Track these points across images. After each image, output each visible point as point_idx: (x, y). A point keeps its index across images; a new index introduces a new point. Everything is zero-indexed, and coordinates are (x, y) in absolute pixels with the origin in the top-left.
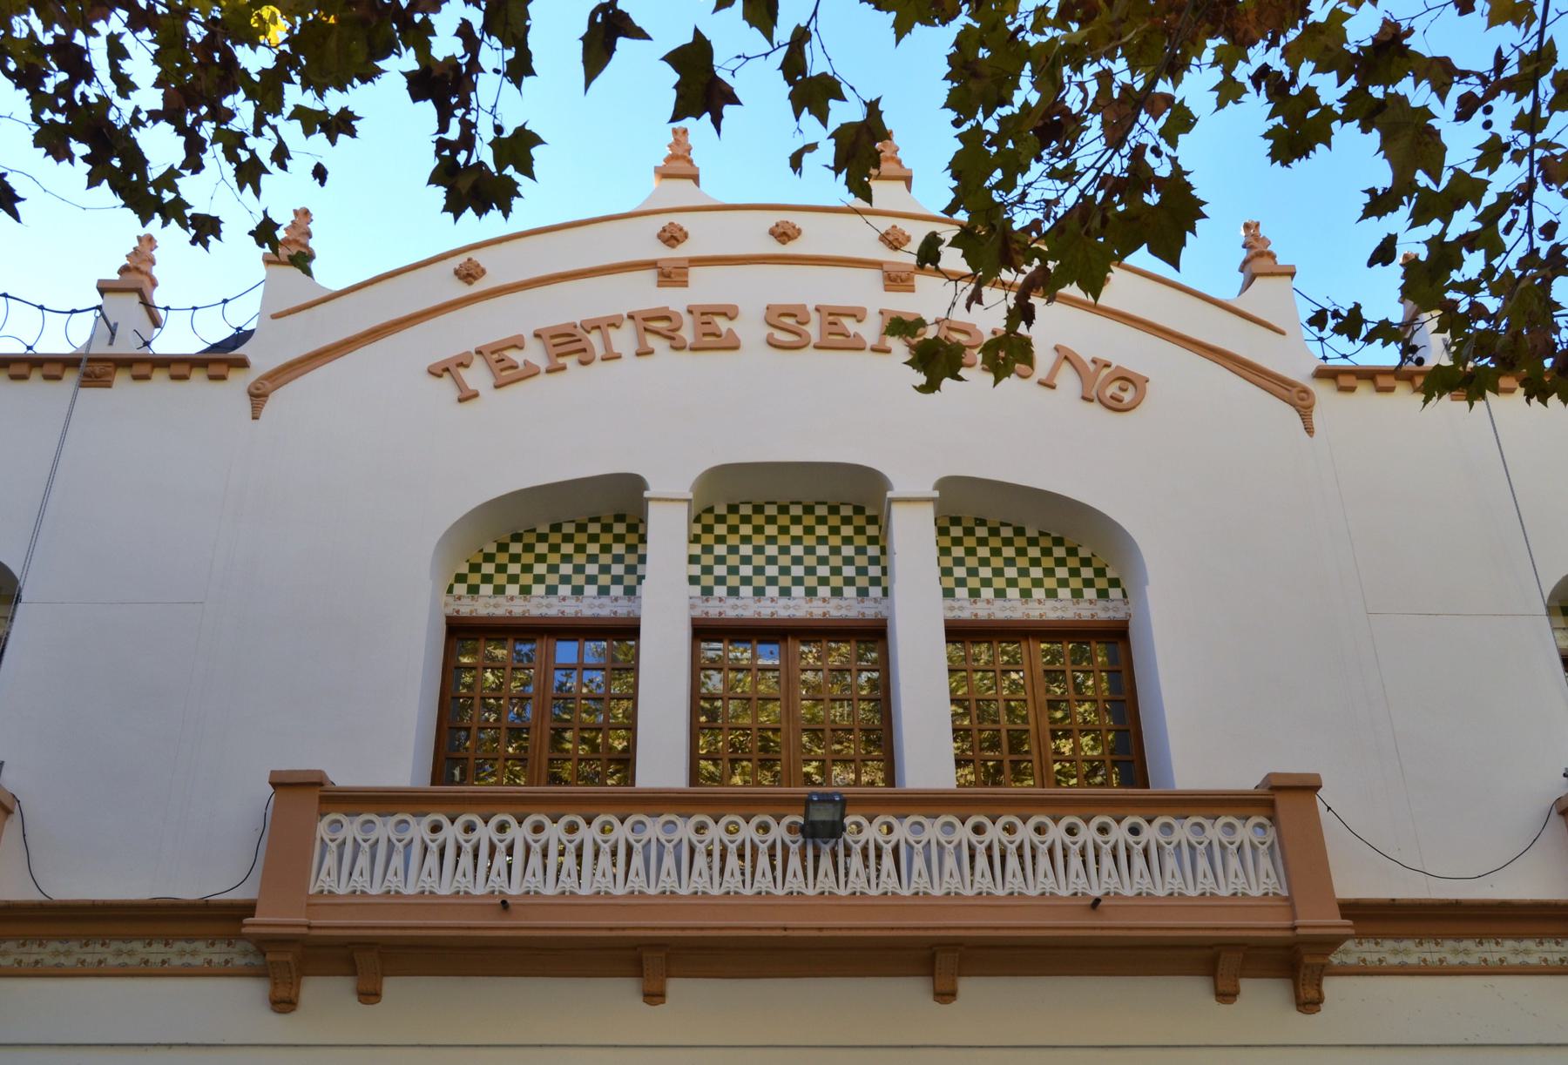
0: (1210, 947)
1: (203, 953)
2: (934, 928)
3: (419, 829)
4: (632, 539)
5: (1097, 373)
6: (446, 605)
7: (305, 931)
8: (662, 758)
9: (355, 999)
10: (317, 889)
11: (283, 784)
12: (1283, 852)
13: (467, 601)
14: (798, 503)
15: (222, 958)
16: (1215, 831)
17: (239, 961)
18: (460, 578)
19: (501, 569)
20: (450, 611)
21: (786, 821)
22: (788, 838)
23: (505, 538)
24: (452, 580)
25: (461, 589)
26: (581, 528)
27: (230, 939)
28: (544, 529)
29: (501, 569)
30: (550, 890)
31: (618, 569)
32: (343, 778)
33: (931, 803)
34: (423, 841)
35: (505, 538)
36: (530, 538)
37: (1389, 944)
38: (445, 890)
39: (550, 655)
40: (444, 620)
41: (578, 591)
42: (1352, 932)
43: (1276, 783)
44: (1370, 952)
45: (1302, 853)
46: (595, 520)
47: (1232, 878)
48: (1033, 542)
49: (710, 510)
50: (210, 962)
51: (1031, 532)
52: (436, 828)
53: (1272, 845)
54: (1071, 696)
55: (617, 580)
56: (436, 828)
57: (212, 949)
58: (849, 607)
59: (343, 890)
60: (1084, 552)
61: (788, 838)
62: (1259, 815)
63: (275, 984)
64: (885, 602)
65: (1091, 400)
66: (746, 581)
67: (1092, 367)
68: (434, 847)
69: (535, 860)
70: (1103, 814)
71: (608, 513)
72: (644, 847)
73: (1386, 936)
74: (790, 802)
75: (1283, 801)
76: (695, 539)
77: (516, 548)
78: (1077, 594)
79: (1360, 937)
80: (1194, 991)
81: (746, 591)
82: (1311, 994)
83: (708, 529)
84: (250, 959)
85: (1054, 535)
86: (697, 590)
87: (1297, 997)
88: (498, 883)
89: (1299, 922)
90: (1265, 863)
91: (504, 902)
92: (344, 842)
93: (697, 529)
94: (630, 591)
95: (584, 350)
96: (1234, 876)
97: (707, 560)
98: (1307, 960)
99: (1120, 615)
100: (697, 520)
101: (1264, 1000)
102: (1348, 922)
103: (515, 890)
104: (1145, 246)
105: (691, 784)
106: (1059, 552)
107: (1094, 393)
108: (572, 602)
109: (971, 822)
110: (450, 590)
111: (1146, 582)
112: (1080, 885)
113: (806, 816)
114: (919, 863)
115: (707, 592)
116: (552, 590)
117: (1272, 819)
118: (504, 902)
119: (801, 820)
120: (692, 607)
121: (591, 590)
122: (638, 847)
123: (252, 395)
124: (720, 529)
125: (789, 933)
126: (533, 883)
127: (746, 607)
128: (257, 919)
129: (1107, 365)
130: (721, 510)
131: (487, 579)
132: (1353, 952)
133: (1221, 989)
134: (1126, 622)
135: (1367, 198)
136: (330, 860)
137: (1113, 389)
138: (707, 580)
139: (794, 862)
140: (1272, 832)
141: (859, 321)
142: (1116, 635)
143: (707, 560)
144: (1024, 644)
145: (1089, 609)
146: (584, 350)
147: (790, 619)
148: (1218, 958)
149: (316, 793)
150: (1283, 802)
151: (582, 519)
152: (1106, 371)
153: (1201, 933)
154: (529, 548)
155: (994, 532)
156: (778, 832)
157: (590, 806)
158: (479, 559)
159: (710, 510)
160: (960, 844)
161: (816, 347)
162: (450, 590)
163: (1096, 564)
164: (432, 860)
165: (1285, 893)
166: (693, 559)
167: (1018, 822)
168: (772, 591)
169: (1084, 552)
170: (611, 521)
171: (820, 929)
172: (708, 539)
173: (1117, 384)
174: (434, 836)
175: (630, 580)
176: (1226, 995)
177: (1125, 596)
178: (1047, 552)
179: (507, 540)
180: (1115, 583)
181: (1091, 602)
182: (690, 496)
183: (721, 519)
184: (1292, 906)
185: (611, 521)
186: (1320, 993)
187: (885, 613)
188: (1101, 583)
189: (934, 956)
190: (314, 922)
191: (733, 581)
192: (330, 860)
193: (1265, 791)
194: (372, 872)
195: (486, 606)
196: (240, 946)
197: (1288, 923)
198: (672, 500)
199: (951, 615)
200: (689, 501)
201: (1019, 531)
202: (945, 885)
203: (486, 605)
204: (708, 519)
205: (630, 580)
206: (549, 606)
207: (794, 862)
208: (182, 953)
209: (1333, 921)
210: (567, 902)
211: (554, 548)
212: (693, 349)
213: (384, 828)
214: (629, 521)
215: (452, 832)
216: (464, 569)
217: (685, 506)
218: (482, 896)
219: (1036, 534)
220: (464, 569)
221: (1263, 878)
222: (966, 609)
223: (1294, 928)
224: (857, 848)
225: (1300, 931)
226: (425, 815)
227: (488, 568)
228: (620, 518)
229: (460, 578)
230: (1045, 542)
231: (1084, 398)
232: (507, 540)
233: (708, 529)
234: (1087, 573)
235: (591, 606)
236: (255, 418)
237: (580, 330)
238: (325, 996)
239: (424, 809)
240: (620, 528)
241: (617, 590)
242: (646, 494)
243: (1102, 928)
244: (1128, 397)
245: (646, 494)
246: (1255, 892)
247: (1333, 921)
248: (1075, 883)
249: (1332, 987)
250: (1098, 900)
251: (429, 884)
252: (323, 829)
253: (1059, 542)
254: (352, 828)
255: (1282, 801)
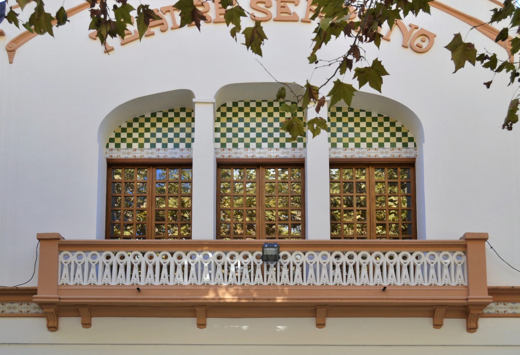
0: (432, 306)
1: (18, 308)
2: (316, 299)
3: (101, 258)
4: (188, 120)
5: (411, 32)
6: (106, 153)
7: (58, 300)
8: (203, 224)
9: (81, 326)
10: (61, 283)
11: (42, 239)
12: (467, 268)
13: (115, 151)
14: (266, 101)
15: (26, 310)
16: (439, 258)
17: (33, 311)
18: (112, 140)
19: (130, 135)
20: (108, 156)
21: (256, 254)
22: (256, 261)
23: (131, 120)
24: (108, 141)
25: (112, 145)
26: (165, 115)
27: (28, 302)
28: (148, 115)
29: (130, 135)
30: (157, 283)
31: (183, 135)
32: (68, 236)
33: (318, 246)
34: (103, 263)
35: (131, 120)
36: (142, 120)
37: (510, 305)
38: (114, 283)
39: (153, 176)
40: (106, 161)
41: (165, 146)
42: (492, 301)
43: (468, 237)
44: (501, 308)
45: (476, 268)
46: (171, 110)
47: (444, 278)
48: (375, 119)
49: (224, 105)
50: (21, 312)
51: (374, 115)
52: (108, 257)
53: (464, 263)
54: (384, 198)
55: (182, 140)
56: (108, 257)
57: (21, 307)
58: (288, 153)
59: (72, 283)
60: (398, 125)
61: (256, 261)
62: (459, 251)
63: (48, 320)
64: (304, 150)
65: (406, 47)
66: (241, 140)
67: (409, 29)
68: (108, 266)
69: (150, 270)
70: (391, 250)
71: (178, 108)
72: (195, 265)
73: (509, 302)
74: (256, 246)
75: (471, 245)
76: (218, 120)
77: (136, 125)
78: (393, 145)
79: (497, 302)
80: (425, 323)
81: (241, 145)
82: (473, 325)
83: (224, 115)
84: (37, 310)
85: (385, 116)
86: (218, 145)
87: (467, 326)
88: (135, 280)
89: (469, 297)
90: (459, 271)
91: (138, 289)
92: (70, 263)
93: (219, 115)
94: (188, 146)
95: (163, 24)
96: (445, 276)
97: (223, 130)
98: (472, 312)
99: (412, 156)
100: (219, 110)
101: (454, 326)
102: (491, 297)
103: (142, 283)
104: (368, 83)
105: (217, 238)
106: (387, 124)
107: (408, 44)
108: (162, 151)
109: (334, 254)
110: (107, 146)
111: (424, 142)
112: (379, 281)
113: (263, 252)
114: (311, 271)
115: (223, 145)
116: (153, 146)
117: (465, 253)
118: (138, 289)
119: (261, 253)
120: (216, 153)
121: (171, 145)
122: (193, 265)
123: (8, 51)
124: (229, 115)
125: (256, 301)
126: (150, 280)
127: (242, 153)
128: (38, 296)
129: (417, 28)
130: (230, 105)
131: (124, 140)
132: (493, 308)
133: (435, 323)
134: (415, 159)
135: (492, 13)
136: (66, 271)
137: (418, 41)
138: (224, 140)
139: (259, 271)
140: (464, 259)
141: (296, 5)
142: (409, 165)
143: (223, 130)
144: (367, 169)
145: (398, 152)
146: (163, 24)
147: (261, 159)
148: (435, 310)
149: (57, 243)
150: (471, 245)
151: (166, 110)
152: (416, 31)
153: (427, 301)
154: (142, 125)
155: (357, 114)
156: (252, 258)
157: (172, 248)
158: (119, 131)
159: (224, 105)
160: (329, 264)
161: (275, 20)
162: (107, 146)
163: (403, 130)
164: (108, 270)
165: (466, 284)
166: (217, 130)
167: (354, 254)
168: (253, 145)
169: (398, 125)
170: (179, 111)
171: (269, 299)
172: (223, 120)
173: (421, 38)
174: (108, 261)
175: (188, 140)
176: (437, 325)
177: (415, 146)
178: (381, 124)
179: (132, 121)
180: (411, 140)
181: (399, 149)
182: (214, 101)
183: (229, 110)
184: (468, 290)
185: (179, 111)
186: (477, 325)
187: (304, 156)
188: (405, 140)
189: (316, 309)
190: (62, 297)
191: (235, 140)
192: (66, 271)
193: (463, 240)
194: (82, 275)
195: (124, 153)
196: (33, 305)
197: (465, 297)
198: (206, 103)
199: (333, 156)
200: (214, 103)
201: (369, 114)
202: (322, 281)
203: (123, 153)
204: (224, 110)
205: (188, 140)
206: (152, 153)
207: (259, 271)
208: (10, 308)
209: (485, 296)
210: (164, 288)
211: (153, 125)
212: (215, 22)
213: (87, 258)
214: (187, 111)
215: (115, 259)
216: (113, 136)
217: (212, 105)
218: (129, 286)
219: (376, 116)
220: (113, 136)
221: (458, 278)
222: (341, 153)
223: (467, 299)
224: (285, 265)
225: (469, 301)
226: (103, 252)
227: (124, 135)
228: (183, 109)
229: (112, 140)
230: (381, 119)
231: (403, 46)
232: (132, 121)
233: (224, 115)
234: (399, 135)
235: (171, 153)
236: (11, 63)
237: (160, 13)
238: (69, 324)
239: (103, 249)
240: (183, 115)
241: (182, 145)
242: (194, 100)
243: (386, 299)
244: (425, 45)
245: (194, 100)
246: (453, 284)
247: (485, 296)
248: (378, 280)
249: (482, 322)
250: (385, 288)
251: (107, 281)
252: (61, 257)
253: (387, 119)
254: (73, 258)
255: (470, 245)
